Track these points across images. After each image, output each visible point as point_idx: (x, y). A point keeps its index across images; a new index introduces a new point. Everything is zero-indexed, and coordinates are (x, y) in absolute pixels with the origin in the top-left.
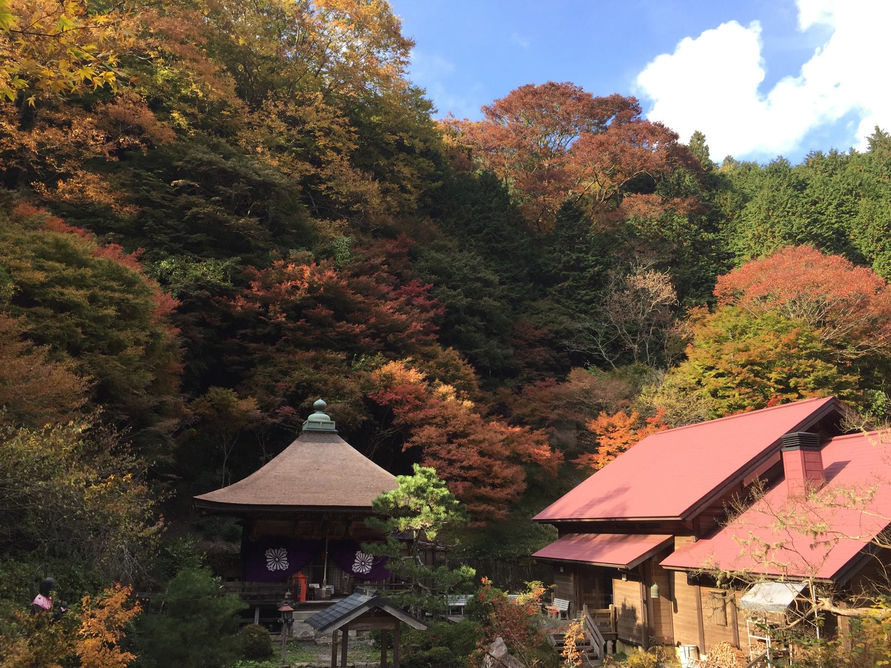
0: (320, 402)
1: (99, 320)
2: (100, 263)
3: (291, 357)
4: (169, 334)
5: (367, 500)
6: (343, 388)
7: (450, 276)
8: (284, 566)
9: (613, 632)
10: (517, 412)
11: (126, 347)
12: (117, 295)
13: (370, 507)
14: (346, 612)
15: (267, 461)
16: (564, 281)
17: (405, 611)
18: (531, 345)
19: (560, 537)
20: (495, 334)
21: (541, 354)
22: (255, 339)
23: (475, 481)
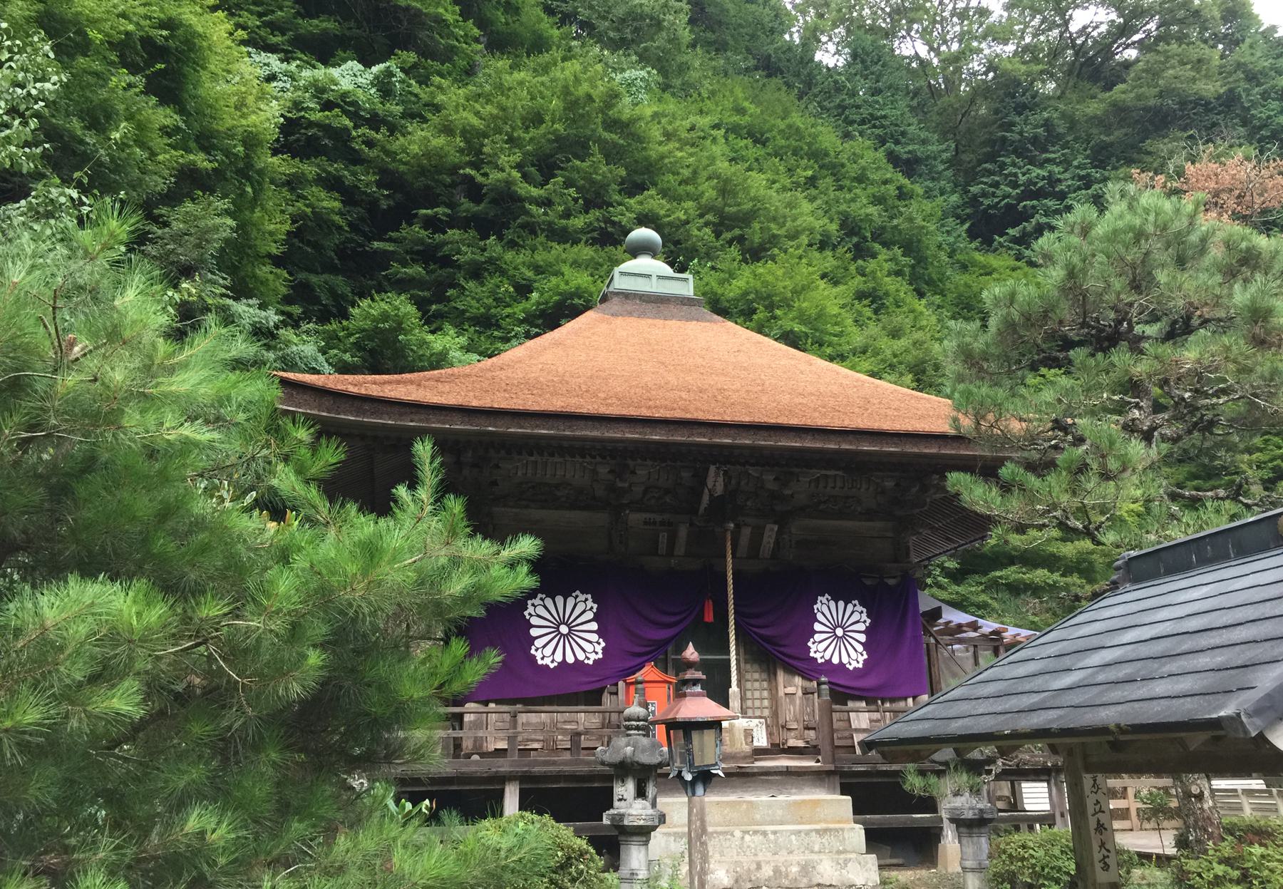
8: (590, 649)
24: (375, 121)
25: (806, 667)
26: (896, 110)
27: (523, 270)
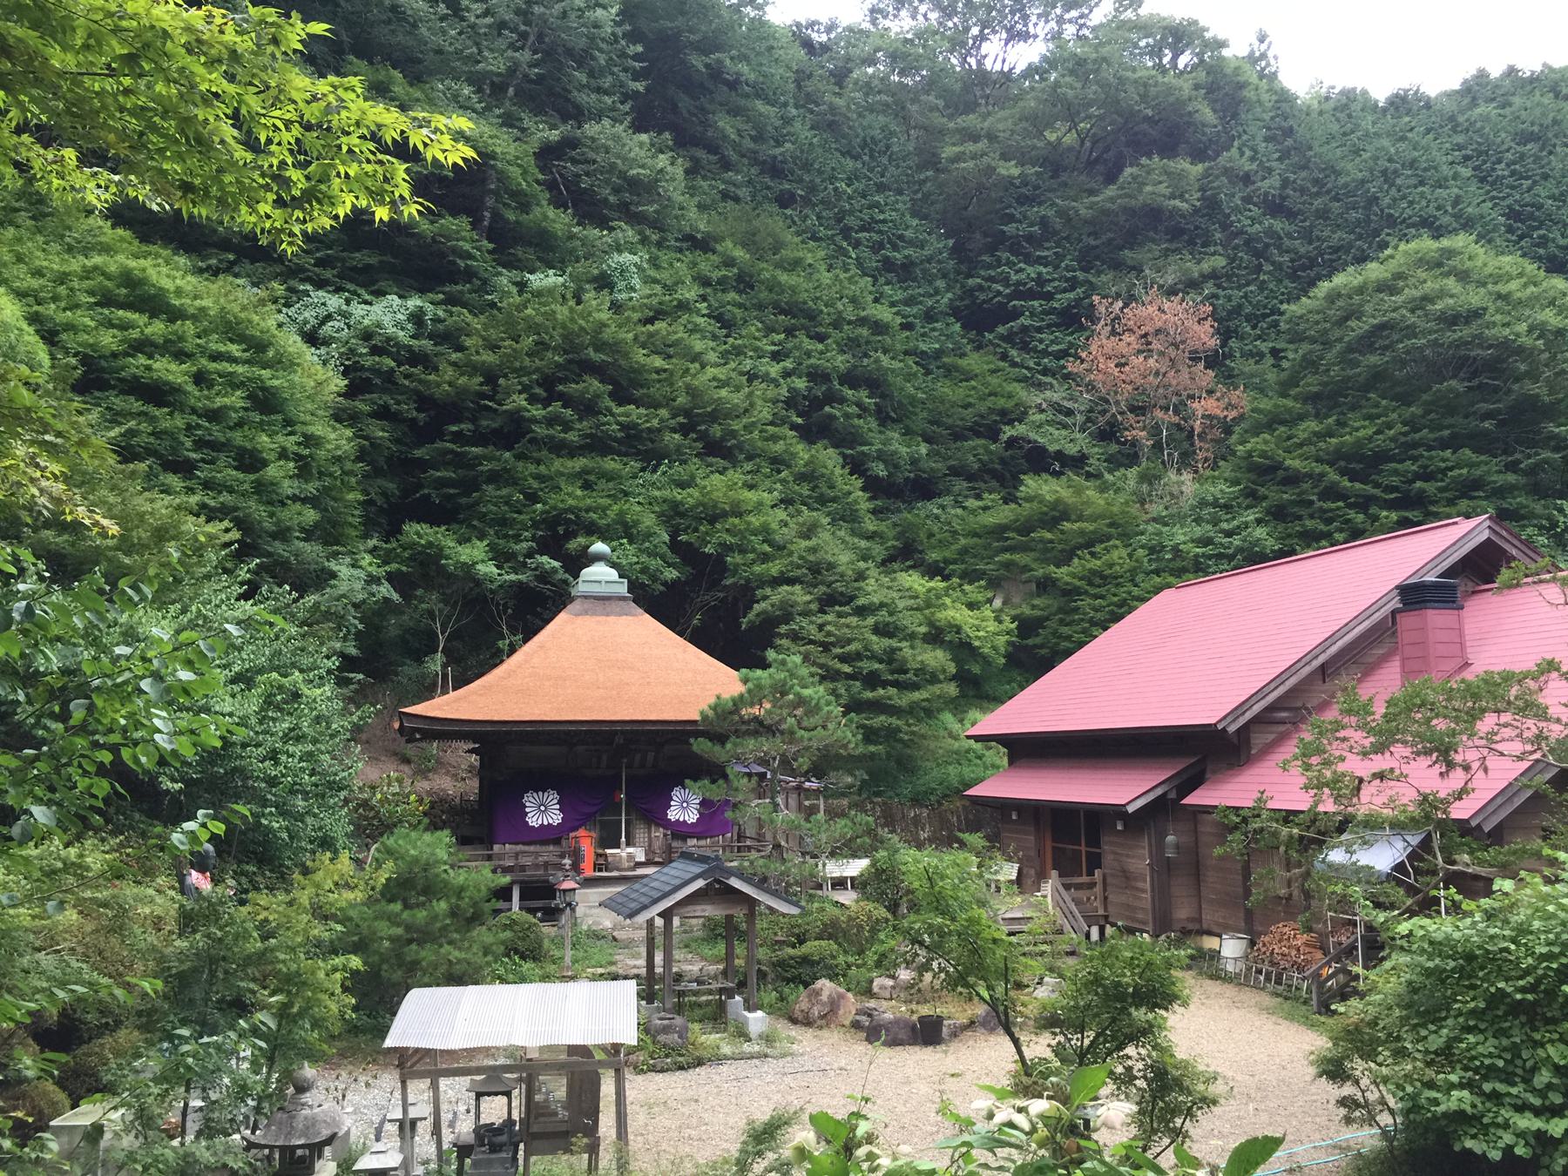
0: (600, 547)
1: (215, 415)
2: (202, 309)
3: (542, 468)
4: (338, 440)
5: (691, 712)
6: (636, 523)
7: (812, 316)
8: (555, 817)
9: (1101, 912)
10: (933, 556)
11: (265, 463)
12: (240, 369)
13: (695, 722)
14: (668, 888)
15: (512, 650)
16: (1014, 319)
17: (762, 883)
18: (958, 436)
19: (1011, 763)
20: (894, 421)
21: (974, 451)
22: (480, 439)
23: (872, 681)
24: (416, 358)
25: (665, 823)
26: (895, 210)
27: (531, 481)
